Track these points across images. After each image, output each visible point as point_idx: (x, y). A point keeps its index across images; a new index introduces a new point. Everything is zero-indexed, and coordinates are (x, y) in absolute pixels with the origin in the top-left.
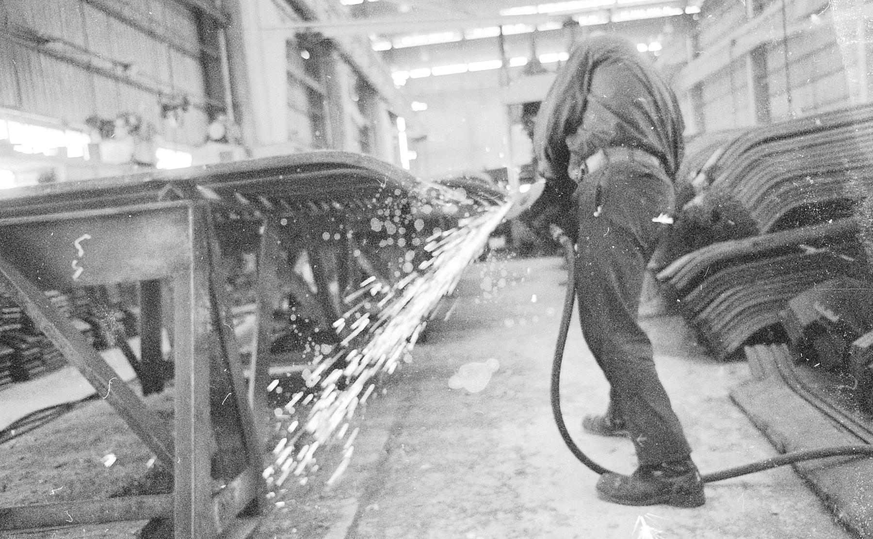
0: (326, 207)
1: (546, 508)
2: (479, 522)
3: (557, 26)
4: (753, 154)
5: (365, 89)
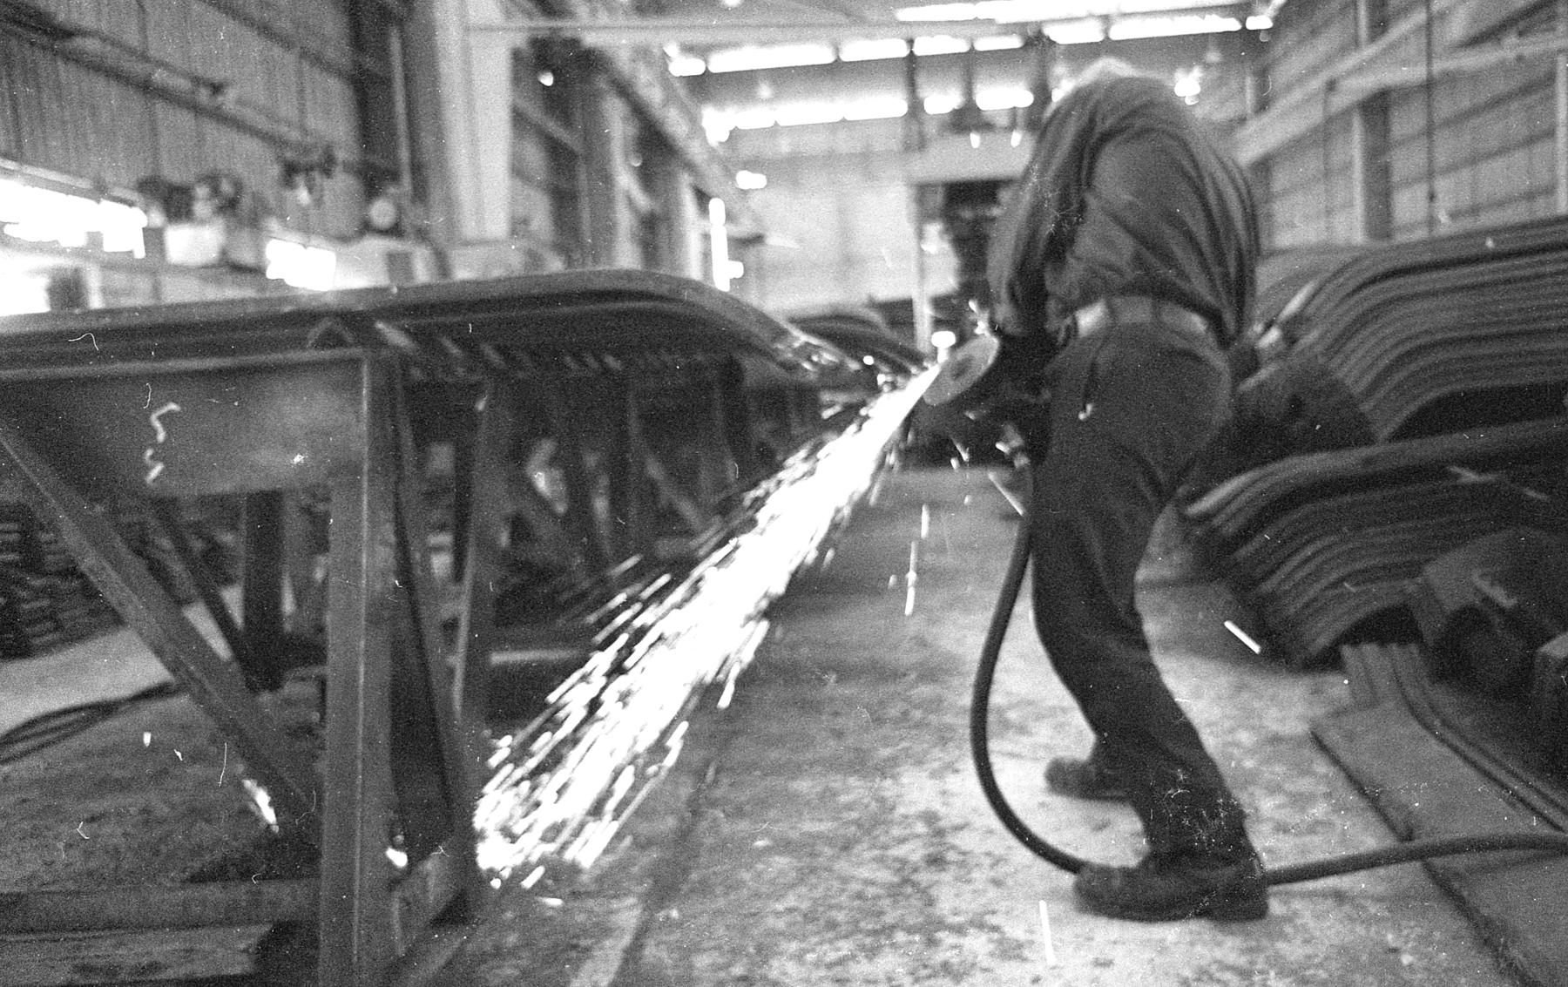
0: (590, 360)
1: (981, 926)
2: (862, 948)
3: (1014, 42)
4: (1374, 295)
5: (656, 149)
